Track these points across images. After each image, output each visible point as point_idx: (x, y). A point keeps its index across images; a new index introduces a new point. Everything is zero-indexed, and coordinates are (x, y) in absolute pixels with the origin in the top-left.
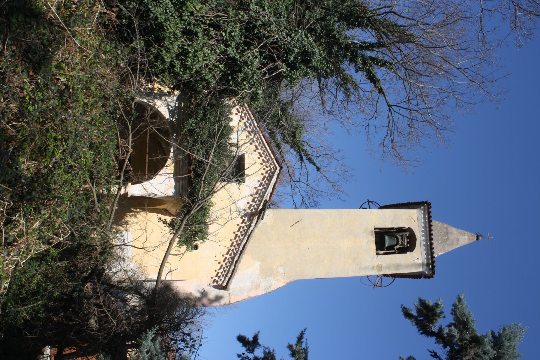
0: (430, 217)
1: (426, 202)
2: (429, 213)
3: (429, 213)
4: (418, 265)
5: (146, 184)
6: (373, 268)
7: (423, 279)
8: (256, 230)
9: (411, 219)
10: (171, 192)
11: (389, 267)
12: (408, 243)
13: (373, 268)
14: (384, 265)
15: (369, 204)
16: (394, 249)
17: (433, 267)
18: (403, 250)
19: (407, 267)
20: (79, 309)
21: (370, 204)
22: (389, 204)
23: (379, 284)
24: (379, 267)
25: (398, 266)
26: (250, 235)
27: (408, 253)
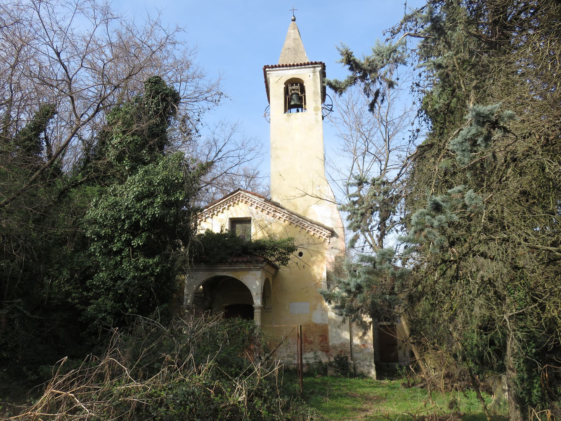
0: (276, 67)
1: (264, 69)
2: (272, 67)
3: (272, 67)
4: (314, 72)
5: (254, 294)
6: (316, 114)
7: (326, 71)
8: (287, 208)
9: (278, 80)
10: (259, 274)
11: (316, 101)
12: (296, 85)
13: (316, 114)
14: (314, 105)
15: (266, 113)
16: (302, 97)
17: (316, 63)
18: (303, 90)
19: (316, 87)
20: (135, 229)
21: (266, 114)
22: (264, 84)
23: (330, 107)
24: (316, 109)
25: (315, 93)
26: (291, 213)
27: (304, 85)
